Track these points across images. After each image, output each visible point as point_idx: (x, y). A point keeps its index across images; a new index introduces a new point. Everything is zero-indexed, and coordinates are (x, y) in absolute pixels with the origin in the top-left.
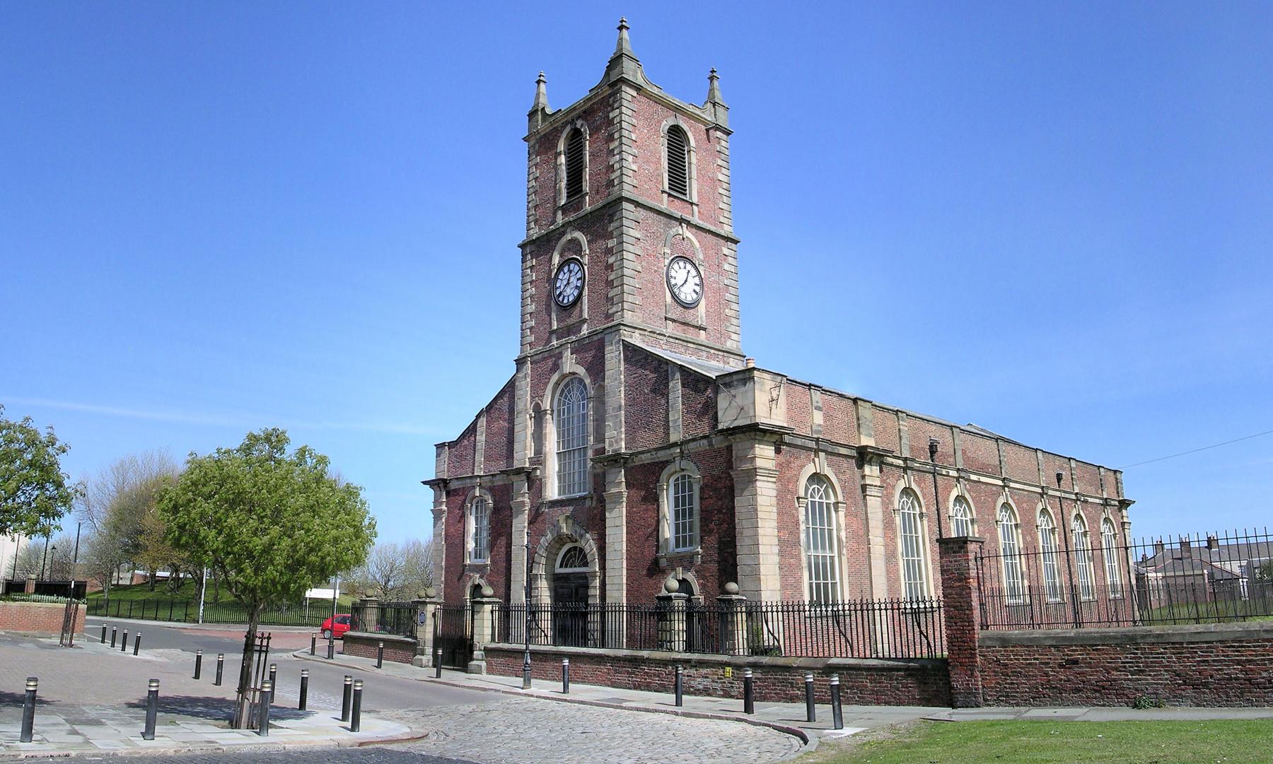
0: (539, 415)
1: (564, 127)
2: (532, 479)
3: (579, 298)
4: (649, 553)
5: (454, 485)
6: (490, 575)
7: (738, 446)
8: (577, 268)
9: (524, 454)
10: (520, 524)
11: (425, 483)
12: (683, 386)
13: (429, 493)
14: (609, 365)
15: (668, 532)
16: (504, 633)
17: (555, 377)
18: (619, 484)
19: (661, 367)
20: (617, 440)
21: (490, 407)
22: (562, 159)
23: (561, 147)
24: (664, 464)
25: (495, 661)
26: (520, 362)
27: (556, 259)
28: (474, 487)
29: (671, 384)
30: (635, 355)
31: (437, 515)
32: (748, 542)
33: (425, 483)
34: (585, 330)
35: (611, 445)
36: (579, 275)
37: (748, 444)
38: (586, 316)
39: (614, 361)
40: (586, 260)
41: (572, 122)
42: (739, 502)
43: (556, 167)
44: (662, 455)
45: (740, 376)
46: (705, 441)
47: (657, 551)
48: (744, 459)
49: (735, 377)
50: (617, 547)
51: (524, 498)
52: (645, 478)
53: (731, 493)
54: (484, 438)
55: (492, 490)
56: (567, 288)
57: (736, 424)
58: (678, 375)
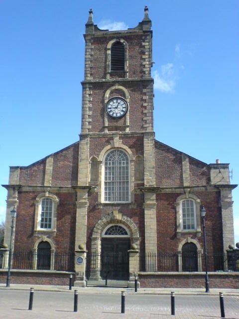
0: (95, 164)
1: (112, 38)
2: (91, 190)
3: (124, 115)
4: (170, 230)
5: (24, 189)
6: (56, 237)
7: (223, 193)
8: (122, 103)
9: (84, 178)
10: (82, 215)
11: (3, 186)
12: (190, 163)
13: (5, 192)
14: (146, 148)
15: (180, 220)
16: (143, 267)
17: (109, 147)
18: (151, 200)
19: (179, 157)
20: (150, 180)
21: (56, 154)
22: (109, 52)
23: (109, 46)
24: (178, 195)
25: (146, 281)
26: (82, 137)
27: (107, 94)
28: (44, 192)
29: (183, 163)
30: (159, 146)
31: (9, 204)
32: (228, 229)
33: (3, 186)
34: (128, 130)
35: (148, 183)
36: (124, 106)
37: (228, 192)
38: (128, 124)
39: (148, 146)
40: (128, 100)
41: (118, 38)
42: (224, 213)
43: (106, 55)
44: (178, 191)
45: (222, 166)
46: (204, 188)
47: (176, 229)
48: (227, 197)
49: (219, 166)
50: (152, 227)
51: (84, 198)
52: (168, 199)
53: (219, 210)
54: (52, 168)
55: (58, 194)
56: (117, 108)
57: (218, 184)
58: (187, 160)
